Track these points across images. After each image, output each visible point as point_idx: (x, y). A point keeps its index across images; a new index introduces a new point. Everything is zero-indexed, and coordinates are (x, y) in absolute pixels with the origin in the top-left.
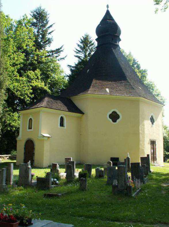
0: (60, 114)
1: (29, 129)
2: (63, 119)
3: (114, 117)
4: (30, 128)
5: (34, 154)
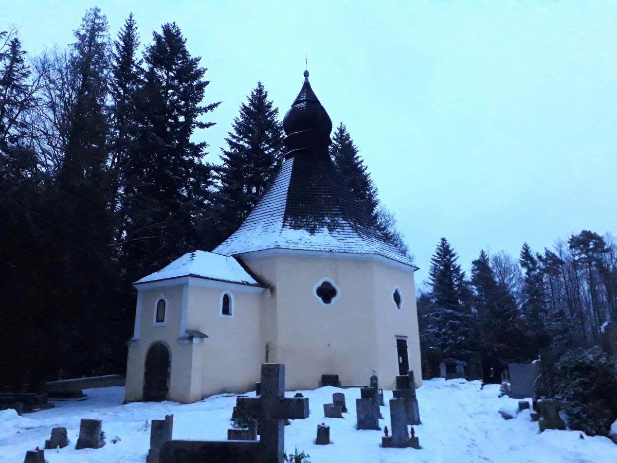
0: (222, 291)
1: (158, 321)
2: (228, 300)
3: (327, 293)
4: (160, 319)
5: (169, 363)
